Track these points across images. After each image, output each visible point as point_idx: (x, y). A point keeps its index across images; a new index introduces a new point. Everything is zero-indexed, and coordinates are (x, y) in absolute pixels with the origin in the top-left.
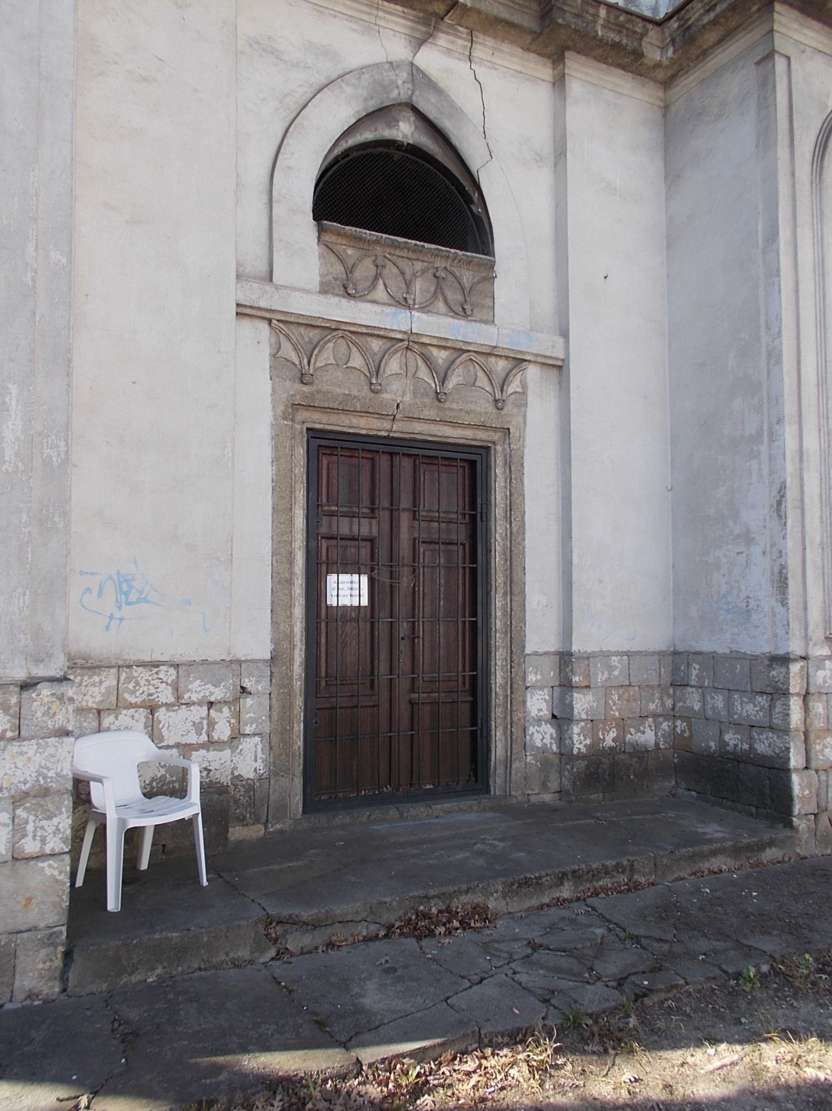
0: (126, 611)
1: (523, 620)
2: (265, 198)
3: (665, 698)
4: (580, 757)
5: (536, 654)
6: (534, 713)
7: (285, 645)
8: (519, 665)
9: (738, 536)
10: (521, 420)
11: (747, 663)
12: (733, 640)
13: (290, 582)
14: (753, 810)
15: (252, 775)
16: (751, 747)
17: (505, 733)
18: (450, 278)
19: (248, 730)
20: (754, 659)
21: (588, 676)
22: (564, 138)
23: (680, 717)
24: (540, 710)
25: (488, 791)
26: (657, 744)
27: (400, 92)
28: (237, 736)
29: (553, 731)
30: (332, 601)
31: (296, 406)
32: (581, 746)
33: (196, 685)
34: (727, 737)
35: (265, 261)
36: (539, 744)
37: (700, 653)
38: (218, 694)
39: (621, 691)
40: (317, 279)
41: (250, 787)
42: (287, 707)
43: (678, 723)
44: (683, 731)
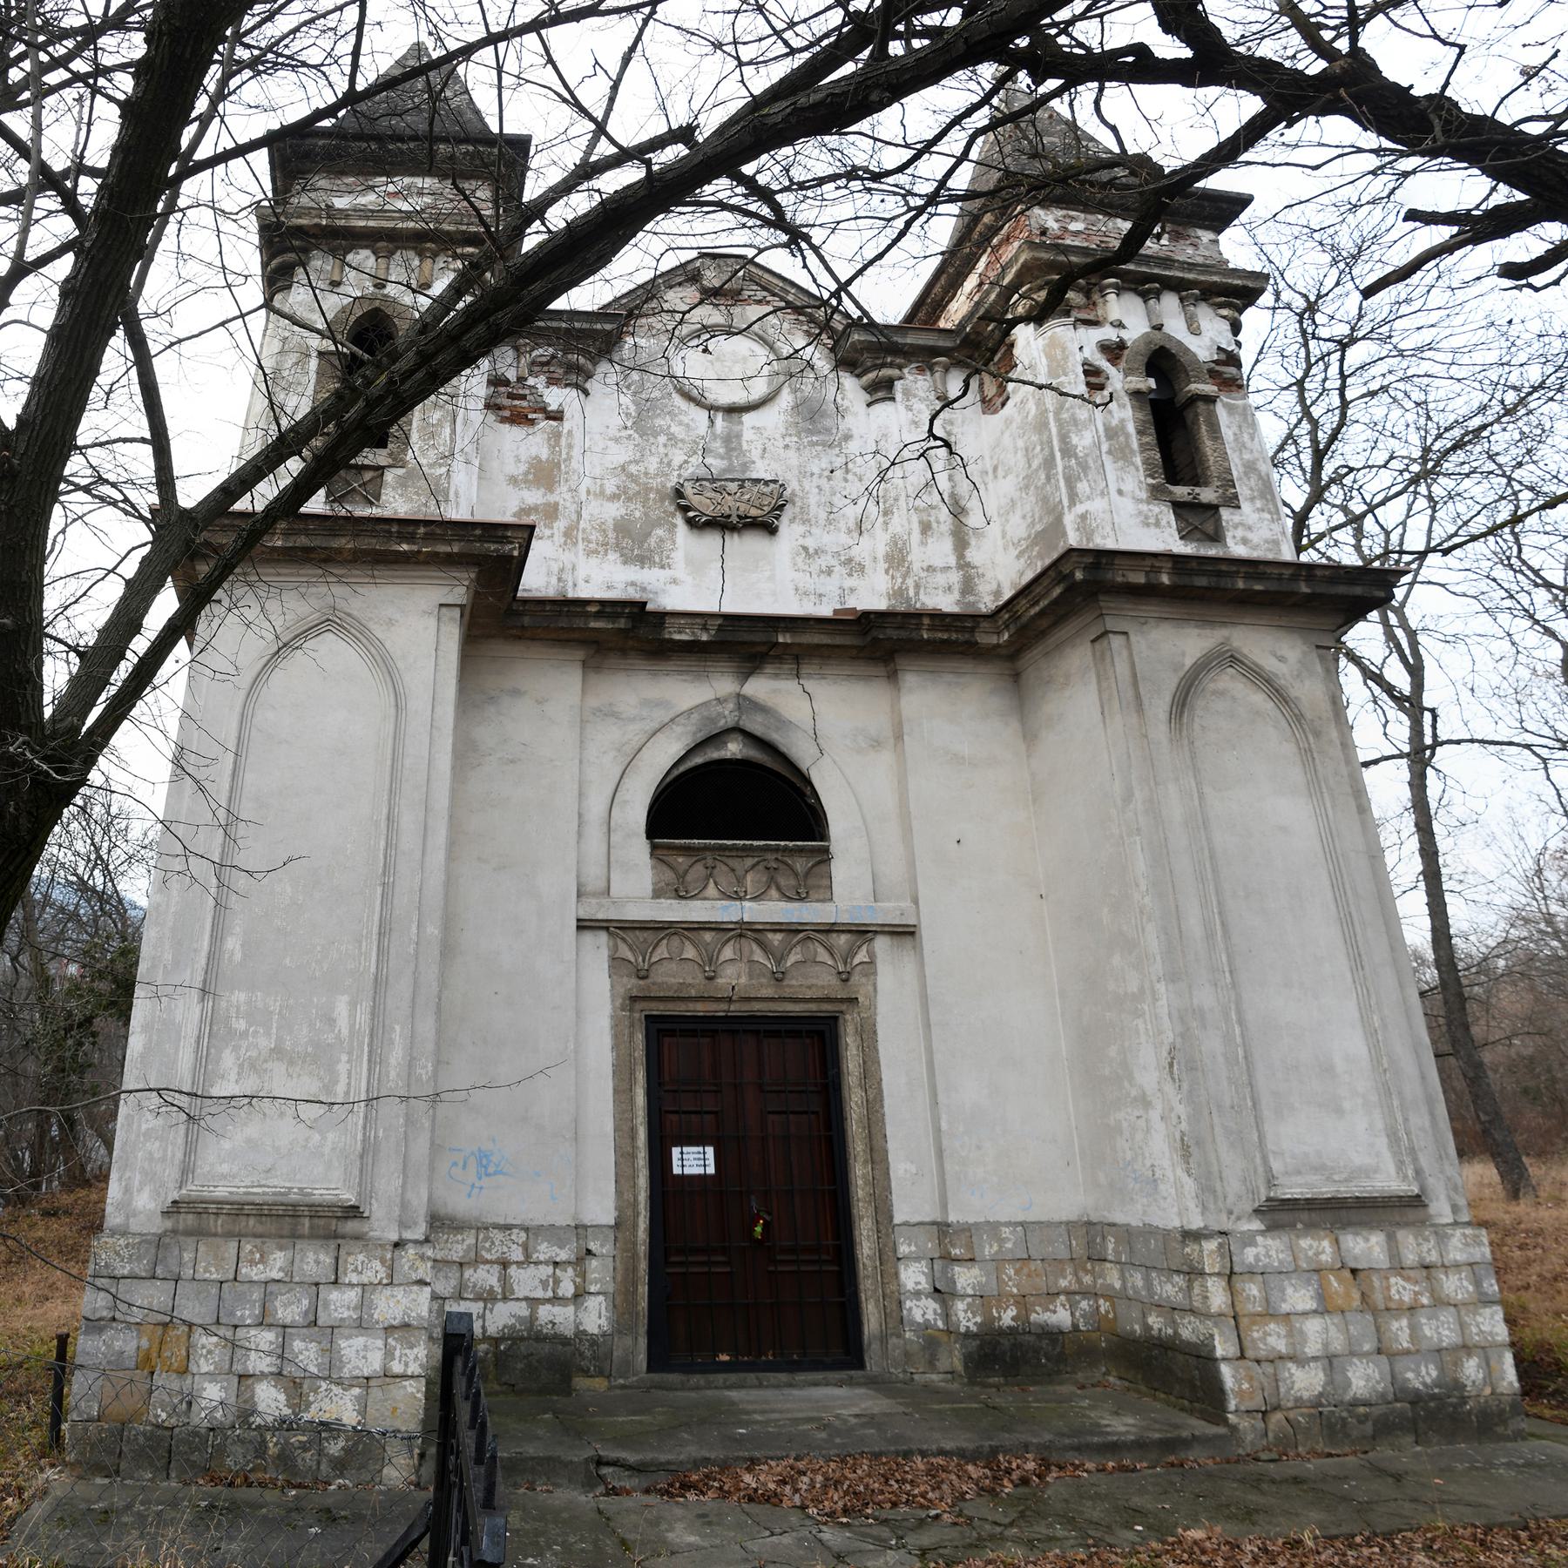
0: (486, 1181)
1: (888, 1189)
2: (605, 829)
3: (1081, 1274)
4: (968, 1335)
5: (906, 1224)
6: (910, 1286)
7: (629, 1212)
8: (887, 1235)
9: (1135, 1099)
10: (870, 988)
11: (1160, 1237)
12: (1145, 1212)
13: (633, 1156)
14: (1186, 1403)
15: (596, 1331)
16: (1176, 1333)
17: (877, 1306)
18: (782, 867)
19: (593, 1289)
20: (1166, 1234)
21: (970, 1246)
22: (900, 724)
23: (1103, 1296)
24: (917, 1283)
25: (861, 1365)
26: (1075, 1327)
27: (728, 715)
28: (580, 1295)
29: (937, 1306)
30: (677, 1170)
31: (634, 999)
32: (970, 1324)
33: (543, 1247)
34: (1151, 1320)
35: (604, 879)
36: (919, 1319)
37: (1114, 1225)
38: (563, 1255)
39: (1018, 1265)
40: (650, 888)
41: (593, 1341)
42: (631, 1270)
43: (1101, 1301)
44: (1107, 1312)
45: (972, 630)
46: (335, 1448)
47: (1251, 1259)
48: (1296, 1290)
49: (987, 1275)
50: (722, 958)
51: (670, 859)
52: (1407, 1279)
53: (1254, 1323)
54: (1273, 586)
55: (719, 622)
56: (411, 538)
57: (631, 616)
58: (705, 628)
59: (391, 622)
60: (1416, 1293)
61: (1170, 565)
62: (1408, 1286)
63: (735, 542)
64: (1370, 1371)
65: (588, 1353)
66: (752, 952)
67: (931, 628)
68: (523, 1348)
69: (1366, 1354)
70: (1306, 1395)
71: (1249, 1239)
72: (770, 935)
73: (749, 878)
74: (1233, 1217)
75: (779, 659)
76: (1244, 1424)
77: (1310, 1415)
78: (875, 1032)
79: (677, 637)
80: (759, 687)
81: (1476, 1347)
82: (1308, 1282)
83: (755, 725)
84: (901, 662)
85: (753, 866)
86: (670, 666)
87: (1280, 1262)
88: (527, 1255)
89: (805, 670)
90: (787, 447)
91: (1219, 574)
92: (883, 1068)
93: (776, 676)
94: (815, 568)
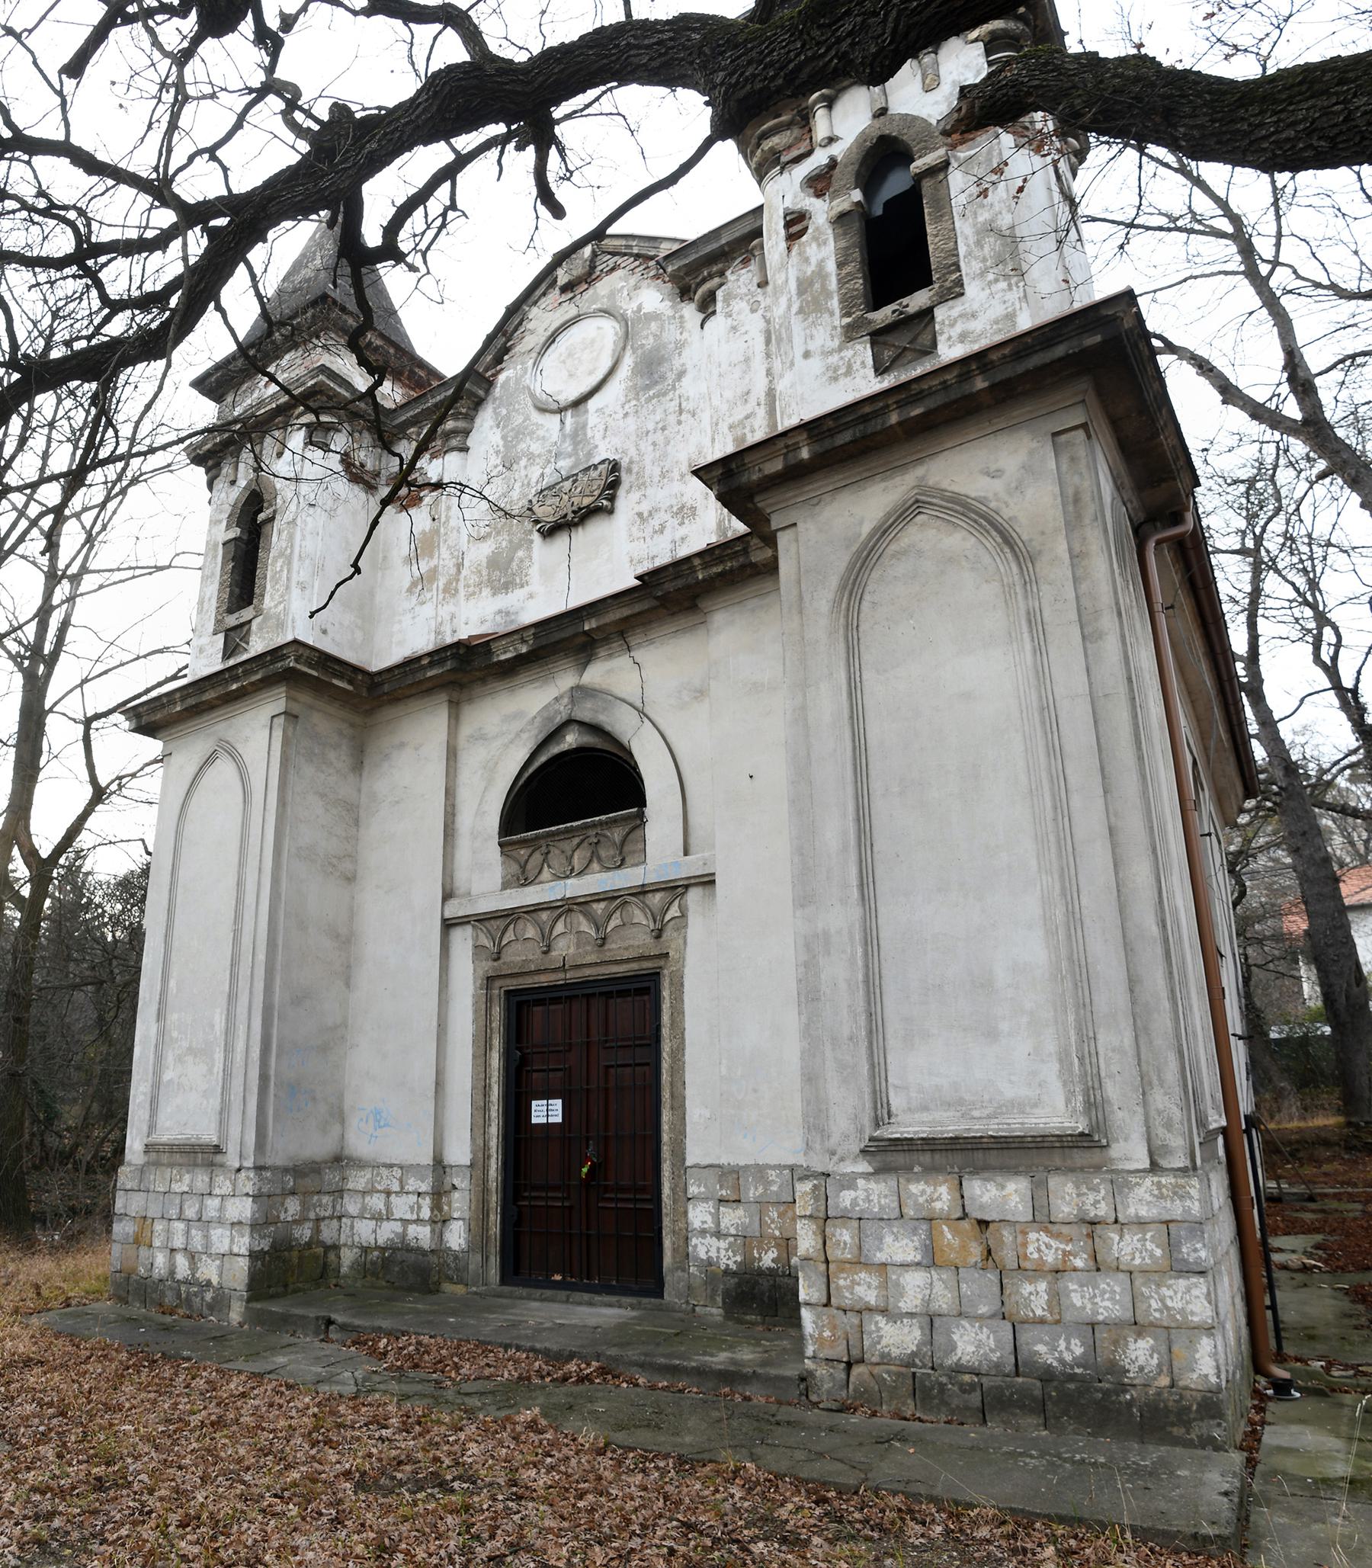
1: (683, 1133)
10: (681, 941)
15: (457, 1248)
25: (660, 1294)
27: (563, 713)
36: (703, 1256)
39: (782, 1209)
42: (484, 1202)
45: (745, 551)
46: (209, 1296)
47: (848, 1203)
48: (896, 1239)
49: (751, 1217)
50: (555, 933)
51: (514, 853)
52: (1057, 1236)
53: (843, 1270)
54: (932, 403)
55: (532, 631)
56: (236, 679)
57: (454, 656)
58: (523, 641)
59: (247, 739)
60: (1065, 1253)
61: (805, 436)
62: (1052, 1242)
63: (580, 536)
64: (983, 1337)
65: (453, 1265)
66: (579, 924)
67: (706, 566)
68: (399, 1256)
69: (980, 1318)
70: (895, 1352)
71: (849, 1182)
72: (595, 906)
73: (576, 856)
74: (835, 1158)
75: (606, 640)
76: (822, 1371)
77: (899, 1375)
78: (682, 985)
79: (503, 657)
80: (596, 674)
81: (1152, 1325)
82: (914, 1231)
83: (585, 713)
84: (703, 604)
85: (578, 845)
86: (522, 678)
87: (881, 1207)
88: (402, 1187)
89: (633, 641)
90: (626, 415)
91: (865, 419)
92: (687, 1018)
93: (610, 656)
94: (649, 530)
